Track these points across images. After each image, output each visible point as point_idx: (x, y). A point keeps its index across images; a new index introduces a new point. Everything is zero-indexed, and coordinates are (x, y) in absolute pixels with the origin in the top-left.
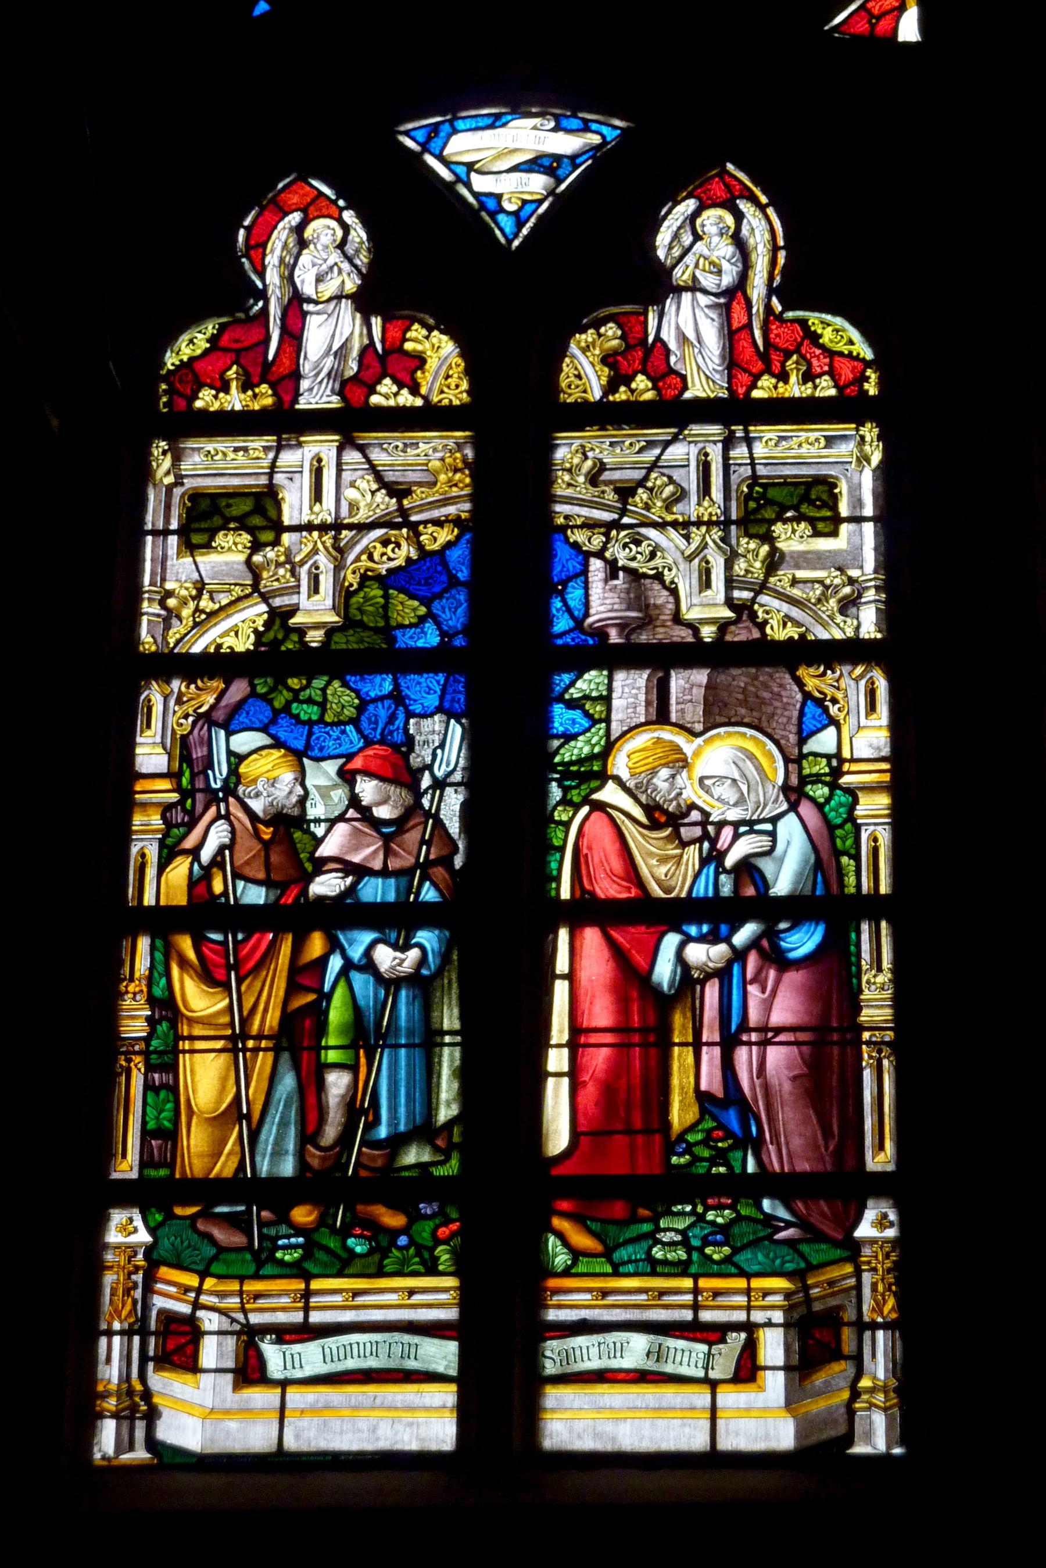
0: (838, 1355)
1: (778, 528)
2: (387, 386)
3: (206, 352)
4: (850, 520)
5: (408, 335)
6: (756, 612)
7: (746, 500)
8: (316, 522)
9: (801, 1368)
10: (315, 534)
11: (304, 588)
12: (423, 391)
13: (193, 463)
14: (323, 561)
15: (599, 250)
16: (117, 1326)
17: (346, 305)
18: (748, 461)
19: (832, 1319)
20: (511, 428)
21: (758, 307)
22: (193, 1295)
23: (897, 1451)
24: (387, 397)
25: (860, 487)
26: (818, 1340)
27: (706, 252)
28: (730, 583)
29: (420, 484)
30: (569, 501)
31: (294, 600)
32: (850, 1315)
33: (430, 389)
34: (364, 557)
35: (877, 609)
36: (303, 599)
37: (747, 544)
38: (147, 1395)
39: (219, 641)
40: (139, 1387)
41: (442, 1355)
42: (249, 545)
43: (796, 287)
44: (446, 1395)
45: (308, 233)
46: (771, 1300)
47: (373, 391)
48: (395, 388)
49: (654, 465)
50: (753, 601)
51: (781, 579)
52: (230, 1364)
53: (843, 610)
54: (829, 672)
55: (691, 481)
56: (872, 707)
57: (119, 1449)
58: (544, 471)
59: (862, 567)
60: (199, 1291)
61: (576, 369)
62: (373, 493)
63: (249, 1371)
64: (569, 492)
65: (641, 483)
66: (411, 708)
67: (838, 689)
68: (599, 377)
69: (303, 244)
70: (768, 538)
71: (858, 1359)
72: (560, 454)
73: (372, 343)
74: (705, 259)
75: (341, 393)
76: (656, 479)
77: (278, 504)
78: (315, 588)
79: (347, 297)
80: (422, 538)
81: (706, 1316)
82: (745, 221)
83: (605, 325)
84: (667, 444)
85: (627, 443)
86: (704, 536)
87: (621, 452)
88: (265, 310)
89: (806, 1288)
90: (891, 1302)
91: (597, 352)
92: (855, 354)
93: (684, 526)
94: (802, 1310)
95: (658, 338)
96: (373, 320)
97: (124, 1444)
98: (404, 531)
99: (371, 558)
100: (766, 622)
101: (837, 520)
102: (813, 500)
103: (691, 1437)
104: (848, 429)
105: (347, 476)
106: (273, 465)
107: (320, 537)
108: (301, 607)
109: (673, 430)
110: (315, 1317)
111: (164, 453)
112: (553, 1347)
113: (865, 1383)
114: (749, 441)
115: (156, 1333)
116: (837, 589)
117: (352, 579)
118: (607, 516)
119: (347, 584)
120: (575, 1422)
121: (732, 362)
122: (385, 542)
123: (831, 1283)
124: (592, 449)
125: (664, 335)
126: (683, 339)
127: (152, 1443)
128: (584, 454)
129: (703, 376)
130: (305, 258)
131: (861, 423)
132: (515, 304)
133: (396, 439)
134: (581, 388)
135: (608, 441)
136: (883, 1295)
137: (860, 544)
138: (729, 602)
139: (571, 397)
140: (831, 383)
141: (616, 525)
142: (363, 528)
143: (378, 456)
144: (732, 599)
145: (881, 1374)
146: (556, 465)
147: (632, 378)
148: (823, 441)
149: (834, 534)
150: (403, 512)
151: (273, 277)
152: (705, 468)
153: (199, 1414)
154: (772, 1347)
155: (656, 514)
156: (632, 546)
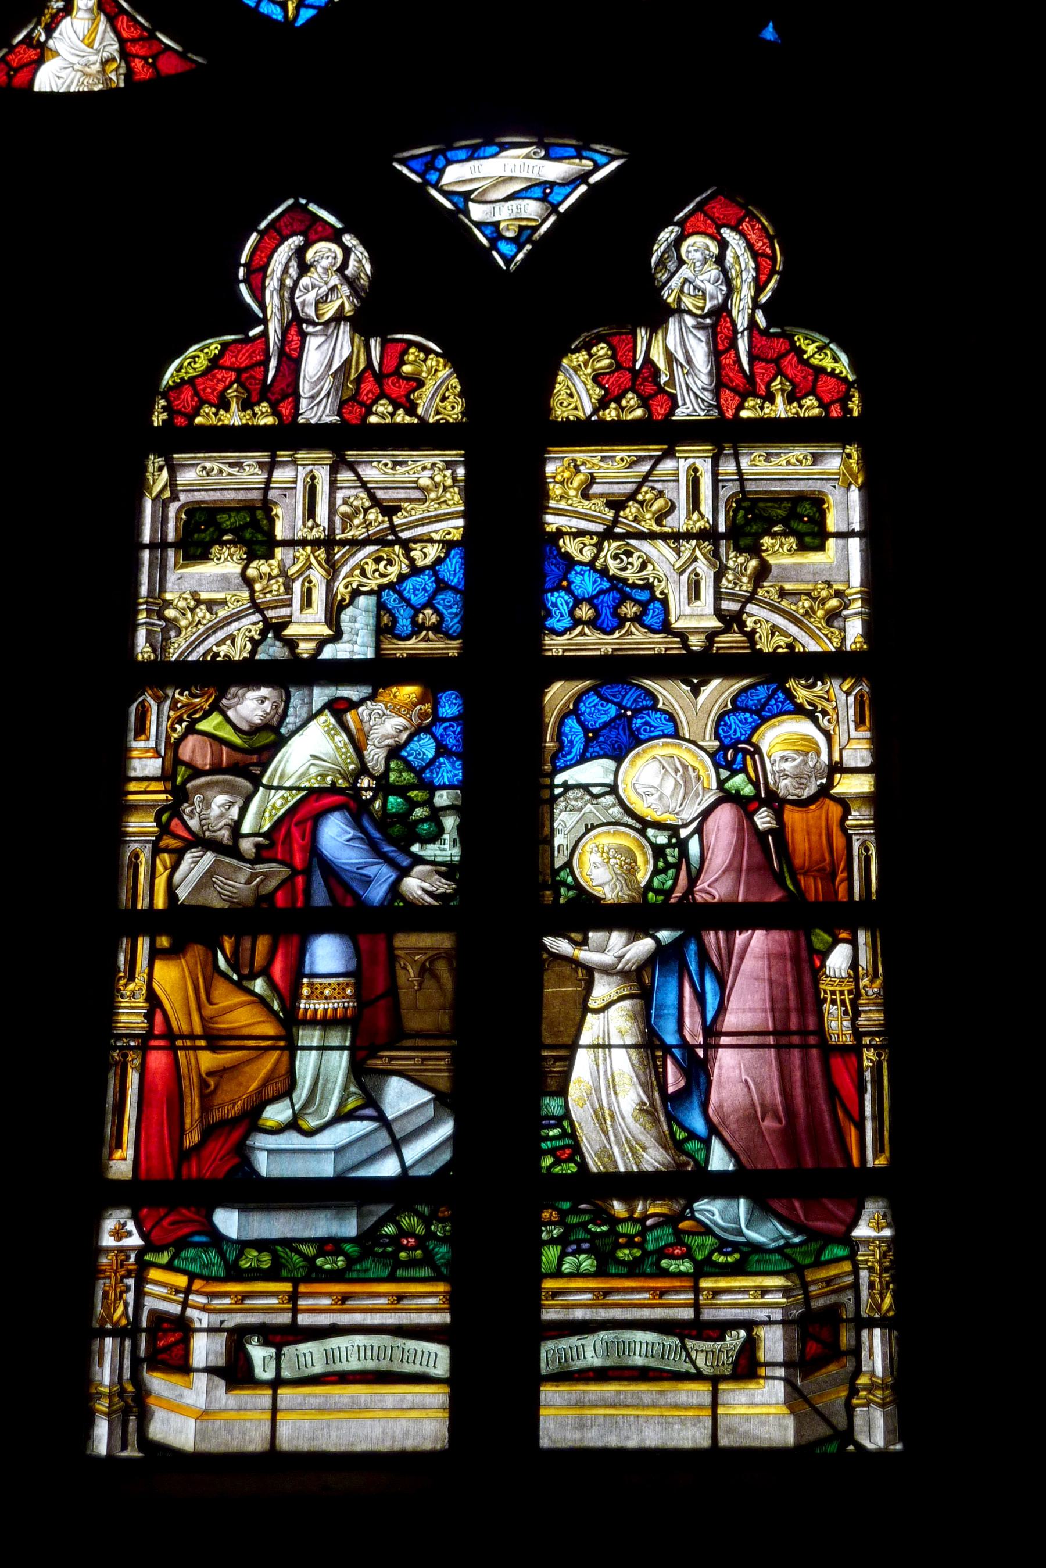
1: (767, 541)
2: (383, 407)
4: (839, 535)
6: (745, 622)
7: (731, 547)
8: (309, 538)
9: (800, 1366)
10: (309, 549)
12: (420, 411)
13: (187, 477)
14: (317, 575)
17: (345, 329)
18: (736, 477)
20: (504, 452)
21: (742, 322)
22: (182, 1295)
23: (899, 1447)
24: (383, 417)
25: (846, 509)
26: (819, 1340)
28: (718, 596)
30: (559, 512)
31: (284, 611)
32: (849, 1313)
33: (427, 410)
34: (357, 572)
35: (863, 620)
37: (734, 560)
39: (215, 649)
41: (437, 1358)
42: (245, 556)
44: (437, 1396)
45: (310, 255)
46: (770, 1298)
47: (370, 412)
48: (390, 409)
50: (742, 611)
51: (768, 590)
54: (819, 683)
61: (568, 387)
64: (562, 505)
65: (632, 497)
67: (828, 700)
69: (304, 268)
70: (755, 550)
72: (550, 468)
74: (690, 283)
76: (646, 493)
77: (272, 521)
78: (307, 601)
79: (346, 319)
80: (412, 554)
83: (596, 344)
84: (658, 460)
85: (618, 459)
86: (694, 549)
87: (613, 467)
88: (265, 334)
89: (805, 1286)
90: (888, 1300)
91: (589, 371)
92: (837, 372)
93: (676, 537)
95: (648, 361)
96: (372, 342)
98: (397, 548)
99: (363, 573)
103: (692, 1436)
106: (269, 481)
107: (313, 552)
108: (294, 619)
110: (303, 1320)
111: (161, 469)
112: (548, 1347)
113: (863, 1380)
114: (736, 456)
116: (824, 601)
118: (600, 528)
119: (339, 598)
121: (720, 382)
122: (378, 560)
123: (828, 1281)
124: (584, 464)
126: (670, 357)
127: (145, 1442)
128: (576, 467)
132: (505, 329)
133: (386, 456)
137: (844, 562)
138: (718, 613)
139: (561, 412)
140: (816, 403)
141: (609, 534)
142: (357, 544)
143: (369, 473)
144: (721, 610)
145: (879, 1370)
147: (623, 395)
149: (821, 548)
150: (393, 528)
151: (272, 300)
152: (695, 484)
153: (187, 1414)
154: (773, 1344)
155: (645, 527)
156: (624, 557)
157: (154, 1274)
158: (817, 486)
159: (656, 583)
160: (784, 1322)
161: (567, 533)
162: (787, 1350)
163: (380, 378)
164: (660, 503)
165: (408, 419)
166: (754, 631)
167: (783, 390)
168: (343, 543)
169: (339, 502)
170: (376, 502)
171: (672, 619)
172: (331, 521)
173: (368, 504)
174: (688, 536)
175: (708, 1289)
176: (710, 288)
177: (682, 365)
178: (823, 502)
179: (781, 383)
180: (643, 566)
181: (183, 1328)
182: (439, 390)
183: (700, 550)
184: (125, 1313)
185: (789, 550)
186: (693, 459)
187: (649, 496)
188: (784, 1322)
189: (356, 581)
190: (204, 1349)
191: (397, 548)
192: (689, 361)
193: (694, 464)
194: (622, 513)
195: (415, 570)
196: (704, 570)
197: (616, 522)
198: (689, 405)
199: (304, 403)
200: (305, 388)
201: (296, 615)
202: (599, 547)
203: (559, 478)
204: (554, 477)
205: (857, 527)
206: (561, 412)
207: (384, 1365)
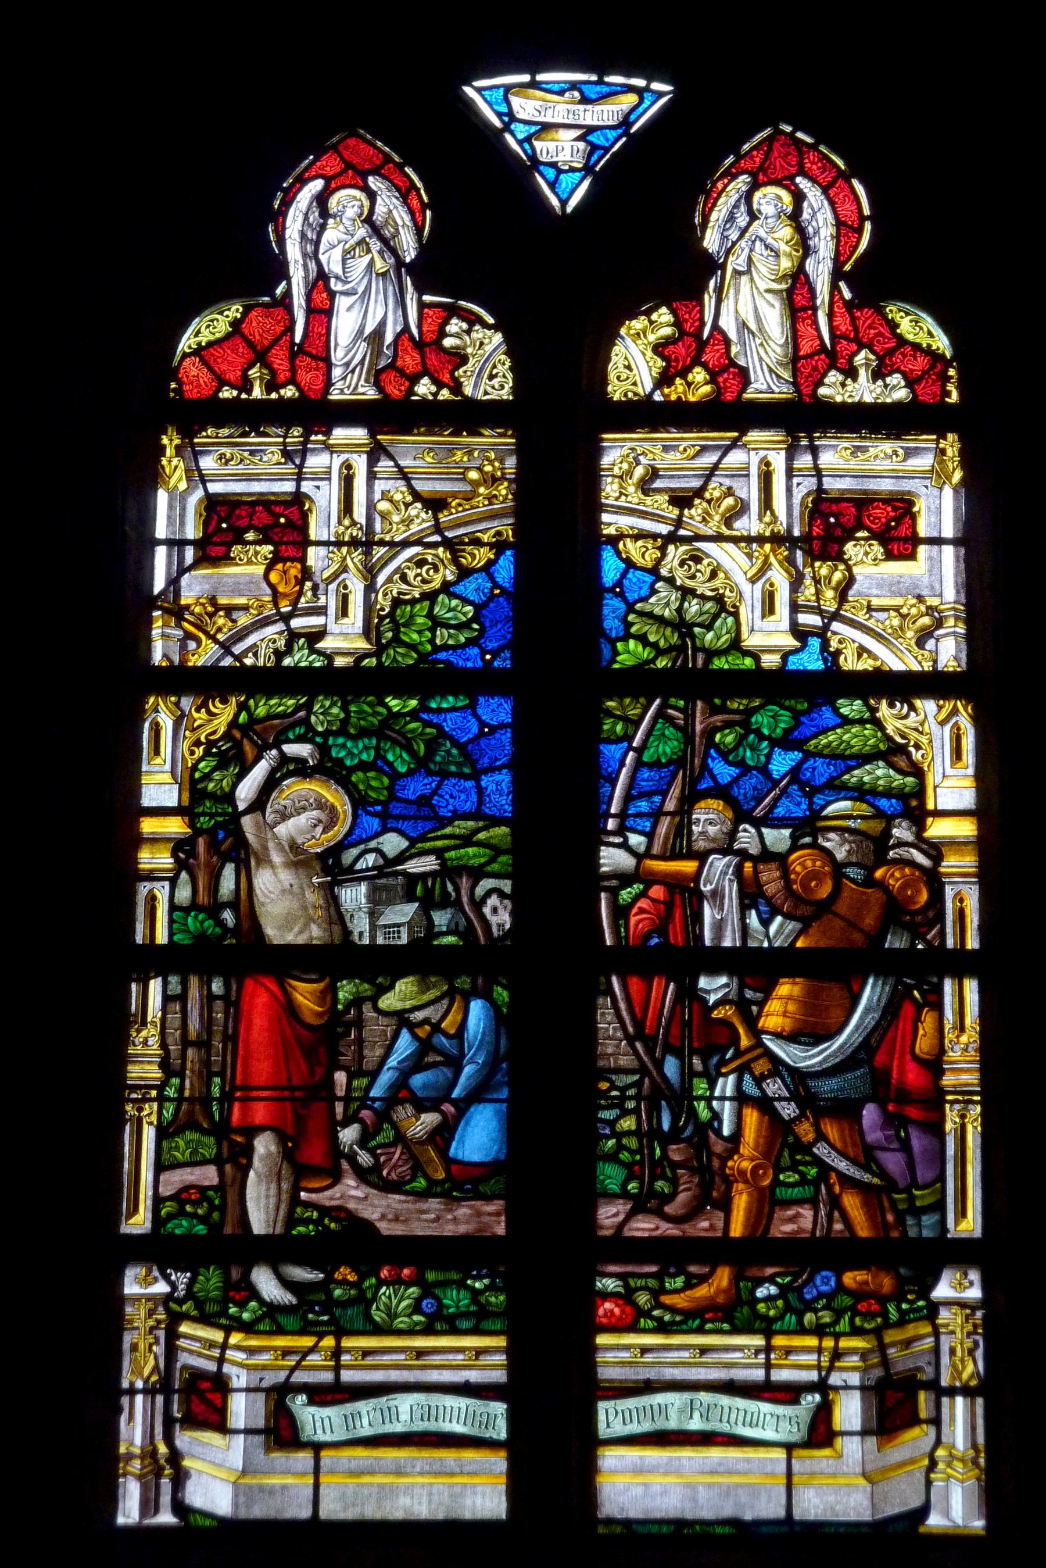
0: (915, 1421)
3: (228, 336)
5: (448, 328)
15: (649, 233)
16: (139, 1384)
20: (559, 426)
25: (939, 511)
26: (895, 1405)
27: (762, 233)
28: (795, 608)
29: (454, 495)
38: (175, 1457)
40: (162, 1449)
45: (333, 202)
49: (712, 471)
52: (261, 1423)
53: (920, 643)
56: (957, 753)
58: (591, 477)
59: (941, 595)
60: (224, 1346)
63: (280, 1432)
65: (699, 493)
66: (618, 1283)
67: (921, 733)
68: (650, 368)
71: (936, 1421)
73: (406, 328)
82: (805, 204)
84: (727, 450)
85: (681, 448)
87: (677, 454)
88: (288, 293)
89: (882, 1348)
94: (878, 1372)
97: (149, 1505)
99: (404, 578)
101: (915, 540)
104: (927, 441)
109: (736, 434)
110: (346, 1376)
114: (814, 451)
118: (664, 529)
125: (723, 323)
126: (743, 326)
127: (180, 1508)
129: (767, 381)
130: (331, 235)
135: (659, 445)
136: (962, 1360)
137: (938, 573)
139: (616, 391)
141: (672, 538)
146: (604, 470)
149: (912, 556)
154: (849, 1412)
157: (184, 1328)
158: (906, 486)
159: (728, 593)
160: (863, 1388)
161: (628, 536)
162: (865, 1420)
163: (420, 345)
167: (867, 365)
168: (382, 543)
169: (377, 496)
170: (417, 496)
171: (745, 634)
172: (370, 519)
173: (409, 498)
174: (761, 540)
176: (784, 248)
177: (753, 334)
178: (912, 504)
179: (866, 358)
180: (714, 575)
182: (486, 363)
183: (775, 556)
184: (156, 1368)
185: (875, 560)
186: (764, 446)
187: (717, 494)
190: (241, 1409)
191: (441, 549)
192: (761, 329)
193: (766, 457)
194: (686, 512)
196: (779, 578)
197: (679, 523)
198: (762, 380)
199: (337, 372)
200: (338, 356)
201: (332, 627)
202: (663, 549)
203: (616, 471)
204: (611, 470)
205: (948, 532)
206: (616, 391)
207: (431, 1426)
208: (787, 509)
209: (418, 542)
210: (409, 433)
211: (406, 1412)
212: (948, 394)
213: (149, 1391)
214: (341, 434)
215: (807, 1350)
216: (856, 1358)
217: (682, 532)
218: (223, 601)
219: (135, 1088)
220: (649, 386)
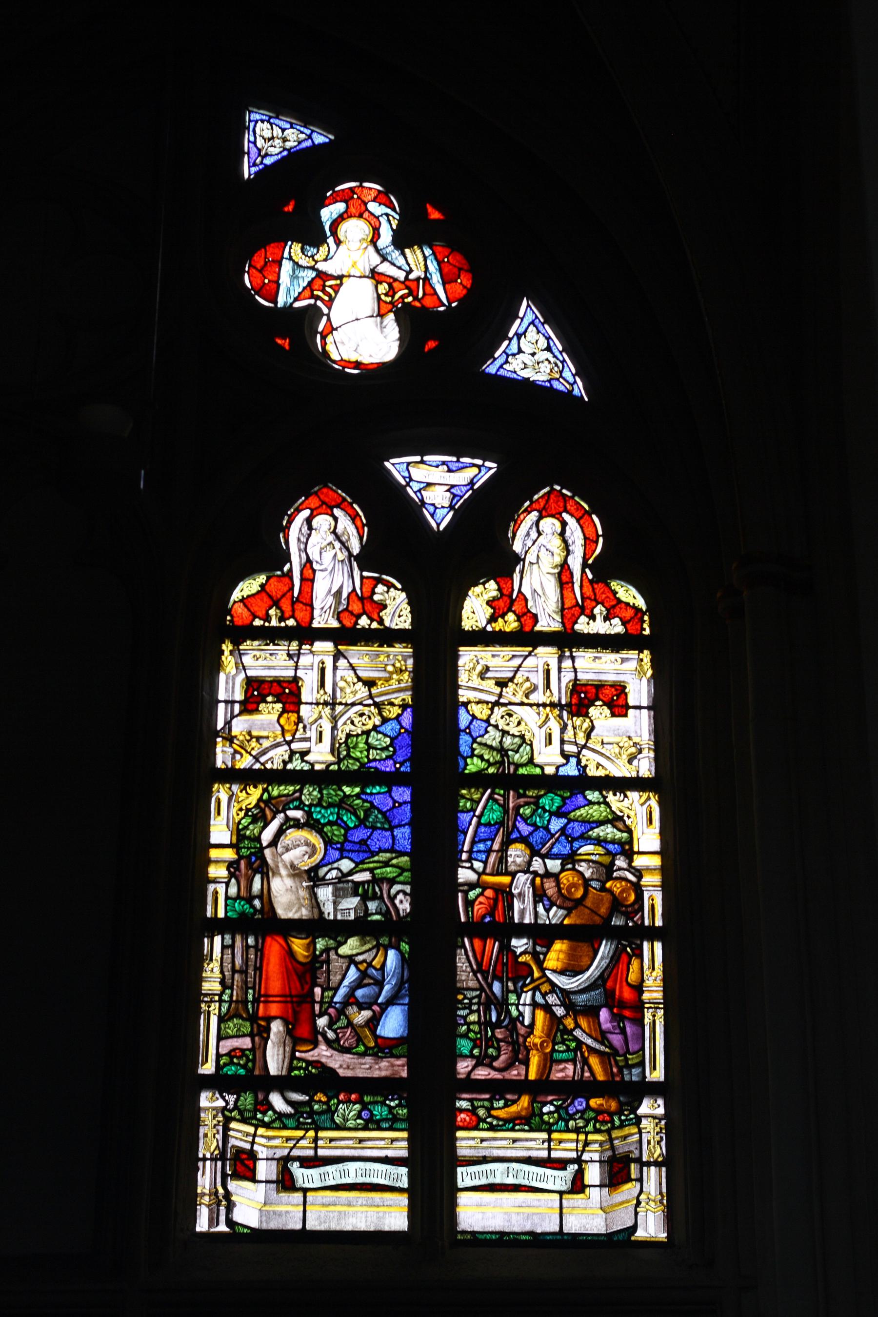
0: (629, 1180)
11: (313, 740)
15: (483, 542)
19: (626, 1160)
20: (436, 643)
25: (639, 691)
26: (618, 1171)
28: (562, 742)
29: (380, 679)
34: (349, 722)
36: (312, 745)
38: (228, 1195)
40: (221, 1191)
41: (401, 1176)
43: (602, 570)
52: (274, 1178)
55: (538, 679)
56: (650, 821)
57: (210, 1226)
60: (255, 1135)
62: (354, 684)
63: (285, 1182)
65: (511, 679)
71: (640, 1180)
73: (354, 589)
75: (339, 619)
81: (554, 1154)
84: (526, 657)
87: (500, 659)
89: (611, 1140)
94: (609, 1153)
97: (213, 1220)
99: (352, 723)
100: (586, 766)
101: (627, 707)
102: (616, 701)
104: (633, 654)
105: (339, 673)
115: (230, 1159)
117: (342, 737)
120: (477, 1213)
122: (362, 715)
125: (523, 590)
127: (230, 1222)
128: (477, 661)
129: (548, 621)
131: (641, 651)
134: (475, 619)
137: (639, 725)
139: (467, 624)
141: (497, 704)
148: (619, 660)
149: (626, 715)
154: (593, 1174)
156: (507, 717)
160: (600, 1161)
163: (361, 599)
164: (527, 684)
165: (379, 627)
166: (586, 766)
169: (338, 678)
170: (359, 679)
173: (355, 680)
174: (544, 705)
175: (556, 1140)
178: (625, 687)
180: (519, 723)
181: (252, 1156)
182: (397, 610)
186: (547, 654)
188: (600, 1161)
189: (349, 727)
190: (265, 1170)
195: (385, 720)
196: (554, 726)
197: (500, 695)
200: (317, 604)
202: (492, 710)
203: (467, 668)
206: (467, 624)
208: (559, 691)
209: (361, 704)
210: (476, 646)
211: (353, 1172)
212: (644, 630)
213: (214, 1159)
214: (540, 650)
215: (571, 1141)
216: (597, 1145)
217: (502, 701)
218: (254, 733)
219: (206, 995)
220: (484, 623)
